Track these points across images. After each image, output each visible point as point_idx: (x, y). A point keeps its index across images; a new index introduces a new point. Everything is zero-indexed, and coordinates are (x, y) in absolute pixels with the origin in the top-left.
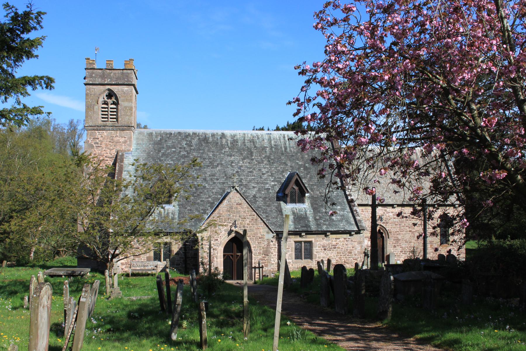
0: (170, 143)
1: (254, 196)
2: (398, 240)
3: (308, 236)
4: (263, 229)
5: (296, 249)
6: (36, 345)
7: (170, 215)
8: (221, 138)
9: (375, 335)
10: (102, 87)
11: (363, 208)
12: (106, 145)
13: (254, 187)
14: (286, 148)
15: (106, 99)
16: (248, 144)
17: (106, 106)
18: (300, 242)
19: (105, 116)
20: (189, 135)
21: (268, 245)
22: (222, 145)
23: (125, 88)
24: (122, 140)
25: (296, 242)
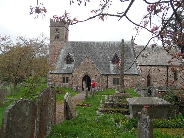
0: (76, 45)
1: (101, 62)
2: (156, 79)
3: (118, 76)
4: (97, 72)
5: (113, 81)
6: (157, 103)
7: (71, 67)
8: (93, 43)
9: (35, 134)
10: (55, 28)
11: (142, 67)
12: (56, 46)
13: (101, 59)
14: (115, 46)
15: (56, 31)
16: (102, 45)
17: (58, 34)
18: (115, 78)
19: (55, 37)
20: (83, 43)
21: (99, 78)
22: (93, 45)
23: (62, 28)
24: (61, 44)
25: (113, 78)
